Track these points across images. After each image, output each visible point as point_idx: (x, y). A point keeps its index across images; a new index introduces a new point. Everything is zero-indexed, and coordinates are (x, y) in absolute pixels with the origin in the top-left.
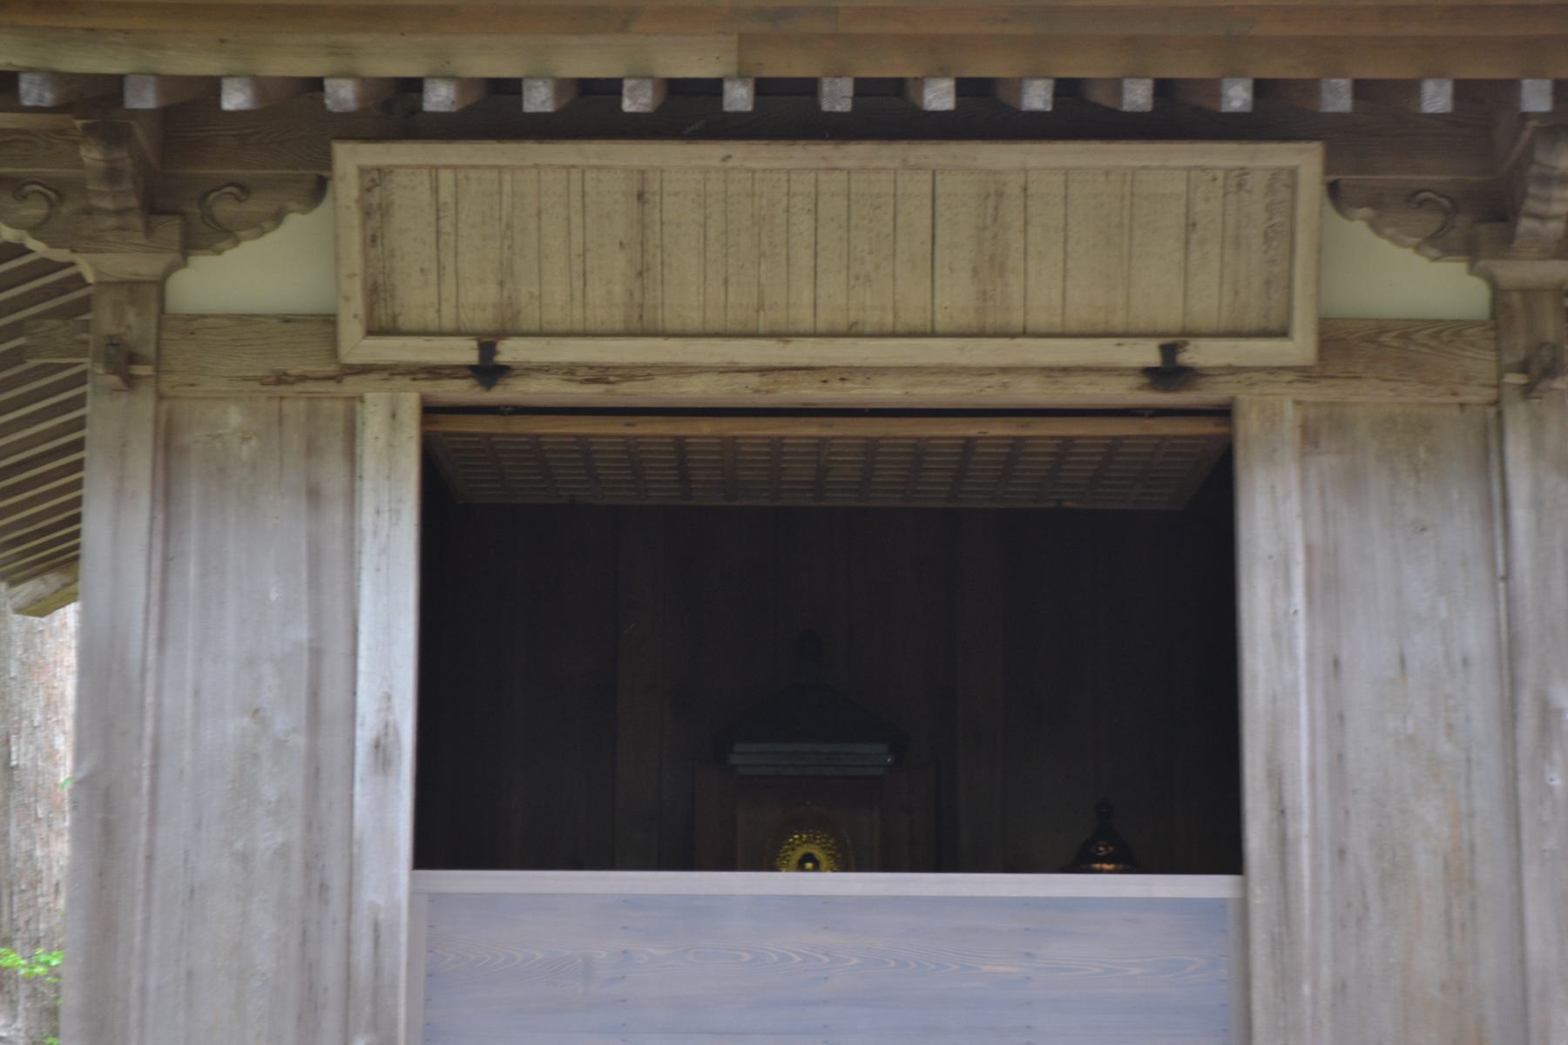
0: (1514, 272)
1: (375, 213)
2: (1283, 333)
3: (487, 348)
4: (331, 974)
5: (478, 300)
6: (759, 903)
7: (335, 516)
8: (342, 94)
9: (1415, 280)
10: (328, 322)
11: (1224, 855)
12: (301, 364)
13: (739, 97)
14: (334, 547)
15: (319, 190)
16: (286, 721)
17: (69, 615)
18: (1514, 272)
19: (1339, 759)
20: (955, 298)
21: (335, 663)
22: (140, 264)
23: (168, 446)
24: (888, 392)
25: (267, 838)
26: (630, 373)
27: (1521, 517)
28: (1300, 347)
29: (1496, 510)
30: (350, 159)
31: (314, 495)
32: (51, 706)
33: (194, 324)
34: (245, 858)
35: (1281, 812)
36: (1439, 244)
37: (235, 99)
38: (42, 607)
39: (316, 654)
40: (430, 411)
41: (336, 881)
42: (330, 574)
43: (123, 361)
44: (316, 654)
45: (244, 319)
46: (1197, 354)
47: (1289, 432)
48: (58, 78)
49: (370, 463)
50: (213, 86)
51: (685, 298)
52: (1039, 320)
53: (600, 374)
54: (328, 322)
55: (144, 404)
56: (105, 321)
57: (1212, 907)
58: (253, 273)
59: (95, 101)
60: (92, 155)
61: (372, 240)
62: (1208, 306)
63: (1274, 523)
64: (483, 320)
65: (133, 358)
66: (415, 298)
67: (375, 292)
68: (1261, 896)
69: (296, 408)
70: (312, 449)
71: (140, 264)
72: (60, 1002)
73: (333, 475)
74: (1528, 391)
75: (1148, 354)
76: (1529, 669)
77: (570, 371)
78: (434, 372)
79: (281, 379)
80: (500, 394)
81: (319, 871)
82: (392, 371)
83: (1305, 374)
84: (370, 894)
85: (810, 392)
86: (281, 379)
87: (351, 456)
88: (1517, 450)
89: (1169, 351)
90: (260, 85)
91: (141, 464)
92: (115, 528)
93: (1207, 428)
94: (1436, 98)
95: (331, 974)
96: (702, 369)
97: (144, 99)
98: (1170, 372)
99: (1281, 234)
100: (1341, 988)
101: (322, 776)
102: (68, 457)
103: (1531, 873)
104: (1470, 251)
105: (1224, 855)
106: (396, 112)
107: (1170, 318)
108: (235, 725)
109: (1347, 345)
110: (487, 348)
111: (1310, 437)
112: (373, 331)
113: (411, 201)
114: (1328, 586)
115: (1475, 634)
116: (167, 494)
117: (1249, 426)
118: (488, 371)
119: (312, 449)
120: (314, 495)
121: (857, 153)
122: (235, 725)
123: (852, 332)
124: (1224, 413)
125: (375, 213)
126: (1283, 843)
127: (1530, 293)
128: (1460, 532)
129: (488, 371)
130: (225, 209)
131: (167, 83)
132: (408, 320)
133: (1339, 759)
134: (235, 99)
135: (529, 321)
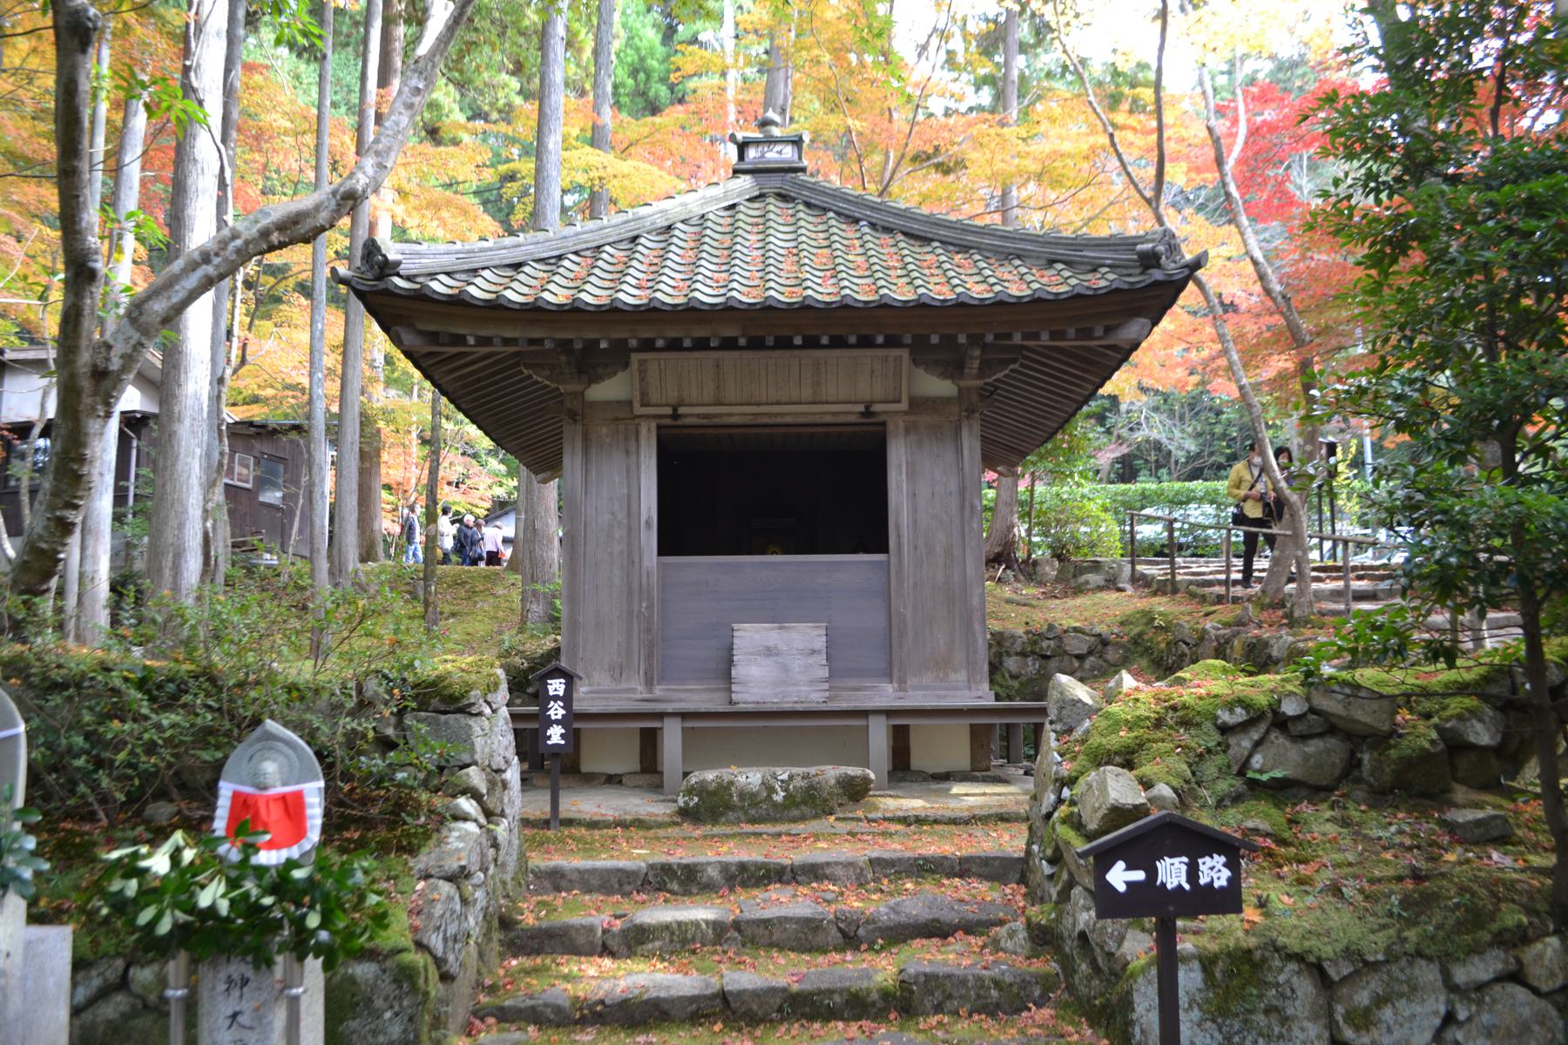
0: (963, 383)
1: (643, 372)
2: (899, 401)
3: (675, 410)
4: (636, 586)
5: (672, 396)
6: (753, 564)
7: (634, 458)
8: (633, 343)
9: (938, 386)
10: (630, 403)
11: (883, 548)
12: (622, 416)
13: (742, 342)
14: (634, 467)
15: (626, 365)
16: (621, 515)
17: (554, 484)
18: (963, 383)
19: (915, 521)
20: (807, 393)
21: (634, 499)
22: (577, 387)
23: (586, 439)
24: (788, 420)
25: (617, 548)
26: (716, 416)
27: (966, 452)
28: (904, 406)
29: (959, 450)
30: (635, 358)
31: (627, 452)
32: (547, 510)
33: (592, 404)
34: (611, 554)
35: (899, 536)
36: (943, 375)
37: (603, 345)
38: (545, 481)
39: (629, 496)
40: (659, 427)
41: (636, 560)
42: (632, 475)
43: (573, 415)
44: (629, 496)
45: (607, 403)
46: (877, 408)
47: (901, 430)
48: (554, 340)
49: (643, 442)
50: (597, 342)
51: (731, 393)
52: (830, 399)
53: (707, 416)
54: (630, 403)
55: (579, 427)
56: (568, 405)
57: (880, 563)
58: (609, 390)
59: (565, 345)
60: (563, 358)
61: (642, 380)
62: (878, 393)
63: (898, 456)
64: (672, 401)
65: (576, 414)
66: (654, 396)
67: (644, 394)
68: (893, 560)
69: (622, 427)
70: (626, 439)
71: (577, 387)
72: (1097, 69)
73: (633, 444)
74: (968, 417)
75: (861, 408)
76: (967, 496)
77: (698, 416)
78: (660, 417)
79: (617, 419)
80: (679, 422)
81: (631, 558)
82: (648, 417)
83: (905, 413)
84: (646, 564)
85: (766, 420)
86: (617, 419)
87: (637, 440)
88: (965, 433)
89: (867, 408)
90: (610, 341)
91: (579, 445)
92: (572, 461)
93: (878, 428)
94: (935, 339)
95: (636, 586)
96: (736, 414)
97: (578, 346)
98: (868, 413)
99: (898, 374)
100: (915, 584)
101: (631, 530)
102: (558, 437)
103: (968, 552)
104: (952, 377)
105: (883, 548)
106: (647, 345)
107: (867, 397)
108: (607, 517)
109: (918, 404)
110: (675, 410)
111: (907, 431)
112: (643, 405)
113: (652, 368)
114: (912, 474)
115: (953, 486)
116: (586, 453)
117: (890, 428)
118: (675, 416)
119: (626, 439)
120: (627, 452)
121: (778, 353)
122: (607, 517)
123: (778, 403)
124: (884, 424)
125: (643, 372)
126: (899, 545)
127: (969, 389)
128: (950, 457)
129: (675, 416)
130: (600, 371)
131: (584, 341)
132: (653, 401)
133: (915, 521)
134: (603, 345)
135: (687, 401)
